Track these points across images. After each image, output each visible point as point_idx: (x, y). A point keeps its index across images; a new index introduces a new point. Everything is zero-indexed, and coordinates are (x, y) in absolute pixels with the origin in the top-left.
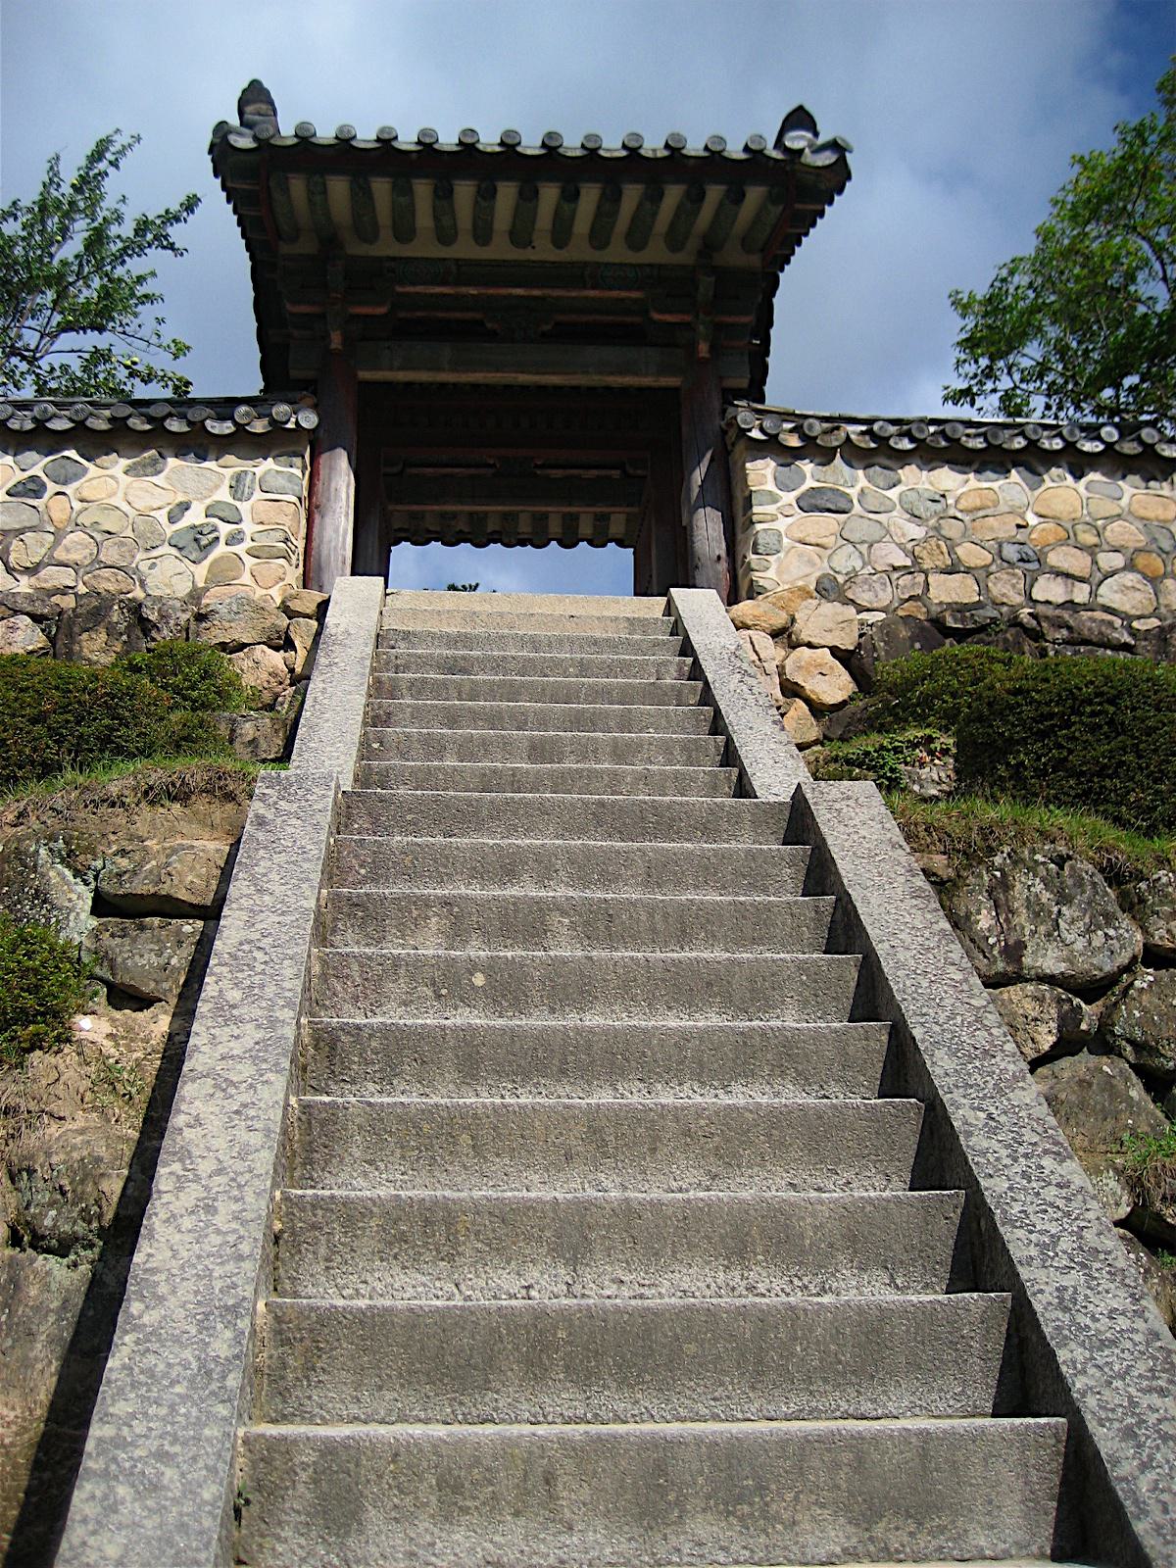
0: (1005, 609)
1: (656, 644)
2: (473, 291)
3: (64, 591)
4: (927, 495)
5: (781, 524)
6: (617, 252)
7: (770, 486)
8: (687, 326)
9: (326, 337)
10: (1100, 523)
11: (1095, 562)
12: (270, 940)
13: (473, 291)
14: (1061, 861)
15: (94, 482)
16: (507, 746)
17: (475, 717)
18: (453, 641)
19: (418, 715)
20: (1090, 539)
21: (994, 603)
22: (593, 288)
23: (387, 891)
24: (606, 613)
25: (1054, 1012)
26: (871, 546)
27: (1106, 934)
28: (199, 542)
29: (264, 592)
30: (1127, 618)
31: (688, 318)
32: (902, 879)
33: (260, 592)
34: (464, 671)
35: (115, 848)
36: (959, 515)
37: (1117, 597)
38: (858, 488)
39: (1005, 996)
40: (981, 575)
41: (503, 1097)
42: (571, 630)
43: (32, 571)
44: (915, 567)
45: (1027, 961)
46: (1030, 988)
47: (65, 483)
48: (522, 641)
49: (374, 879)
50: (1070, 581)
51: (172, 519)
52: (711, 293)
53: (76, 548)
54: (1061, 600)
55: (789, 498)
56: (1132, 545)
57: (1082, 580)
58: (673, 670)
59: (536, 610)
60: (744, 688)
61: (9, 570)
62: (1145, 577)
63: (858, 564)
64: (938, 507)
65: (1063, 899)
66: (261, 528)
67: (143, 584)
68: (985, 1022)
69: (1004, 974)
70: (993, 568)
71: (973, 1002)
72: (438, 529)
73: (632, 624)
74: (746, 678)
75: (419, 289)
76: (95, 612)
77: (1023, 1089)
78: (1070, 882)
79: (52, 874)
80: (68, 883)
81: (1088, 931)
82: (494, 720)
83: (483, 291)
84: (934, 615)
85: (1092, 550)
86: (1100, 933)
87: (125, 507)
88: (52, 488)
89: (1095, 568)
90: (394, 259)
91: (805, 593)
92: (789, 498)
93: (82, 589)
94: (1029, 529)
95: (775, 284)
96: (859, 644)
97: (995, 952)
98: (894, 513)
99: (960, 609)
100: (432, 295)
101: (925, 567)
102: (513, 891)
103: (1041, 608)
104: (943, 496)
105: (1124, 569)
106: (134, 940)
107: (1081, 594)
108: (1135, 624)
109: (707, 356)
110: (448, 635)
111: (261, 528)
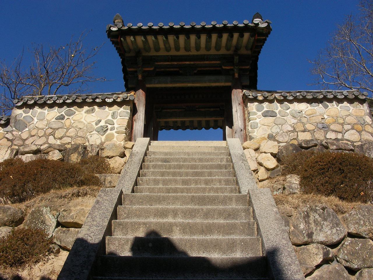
0: (319, 141)
1: (221, 153)
2: (175, 63)
3: (68, 143)
4: (297, 111)
5: (258, 120)
6: (213, 52)
7: (255, 110)
8: (233, 70)
9: (137, 77)
10: (344, 117)
11: (343, 127)
12: (93, 234)
13: (175, 63)
14: (323, 209)
15: (77, 115)
16: (176, 181)
17: (168, 174)
18: (166, 154)
19: (153, 173)
20: (341, 121)
21: (316, 139)
22: (207, 61)
23: (128, 221)
24: (209, 146)
25: (322, 252)
26: (282, 125)
27: (337, 229)
28: (104, 130)
29: (120, 142)
30: (353, 142)
31: (232, 68)
32: (273, 215)
33: (118, 143)
34: (168, 162)
35: (63, 209)
36: (306, 116)
37: (350, 137)
38: (278, 110)
39: (308, 248)
40: (312, 132)
41: (153, 277)
42: (199, 150)
43: (61, 139)
44: (294, 131)
45: (314, 237)
46: (315, 245)
47: (70, 116)
48: (185, 153)
49: (128, 217)
50: (336, 133)
51: (96, 124)
52: (238, 61)
53: (72, 132)
54: (334, 138)
55: (260, 113)
56: (353, 123)
57: (340, 132)
58: (225, 160)
59: (191, 145)
60: (243, 164)
61: (55, 138)
62: (357, 131)
63: (279, 130)
64: (300, 114)
65: (325, 220)
66: (119, 126)
67: (88, 141)
68: (291, 255)
69: (306, 242)
70: (316, 130)
71: (288, 249)
72: (173, 126)
73: (216, 148)
74: (244, 161)
75: (161, 63)
76: (75, 149)
77: (299, 274)
78: (326, 215)
79: (46, 216)
80: (50, 219)
81: (331, 228)
82: (174, 174)
83: (178, 63)
84: (300, 143)
85: (342, 124)
86: (335, 229)
87: (85, 122)
88: (66, 117)
89: (343, 129)
90: (154, 56)
91: (264, 139)
92: (260, 113)
93: (73, 143)
94: (325, 119)
95: (257, 59)
96: (278, 152)
97: (305, 235)
98: (288, 116)
99: (307, 142)
100: (165, 65)
101: (297, 130)
102: (165, 220)
103: (329, 140)
104: (302, 111)
105: (351, 129)
106: (66, 234)
107: (340, 136)
108: (355, 144)
109: (238, 77)
110: (165, 152)
111: (119, 126)
